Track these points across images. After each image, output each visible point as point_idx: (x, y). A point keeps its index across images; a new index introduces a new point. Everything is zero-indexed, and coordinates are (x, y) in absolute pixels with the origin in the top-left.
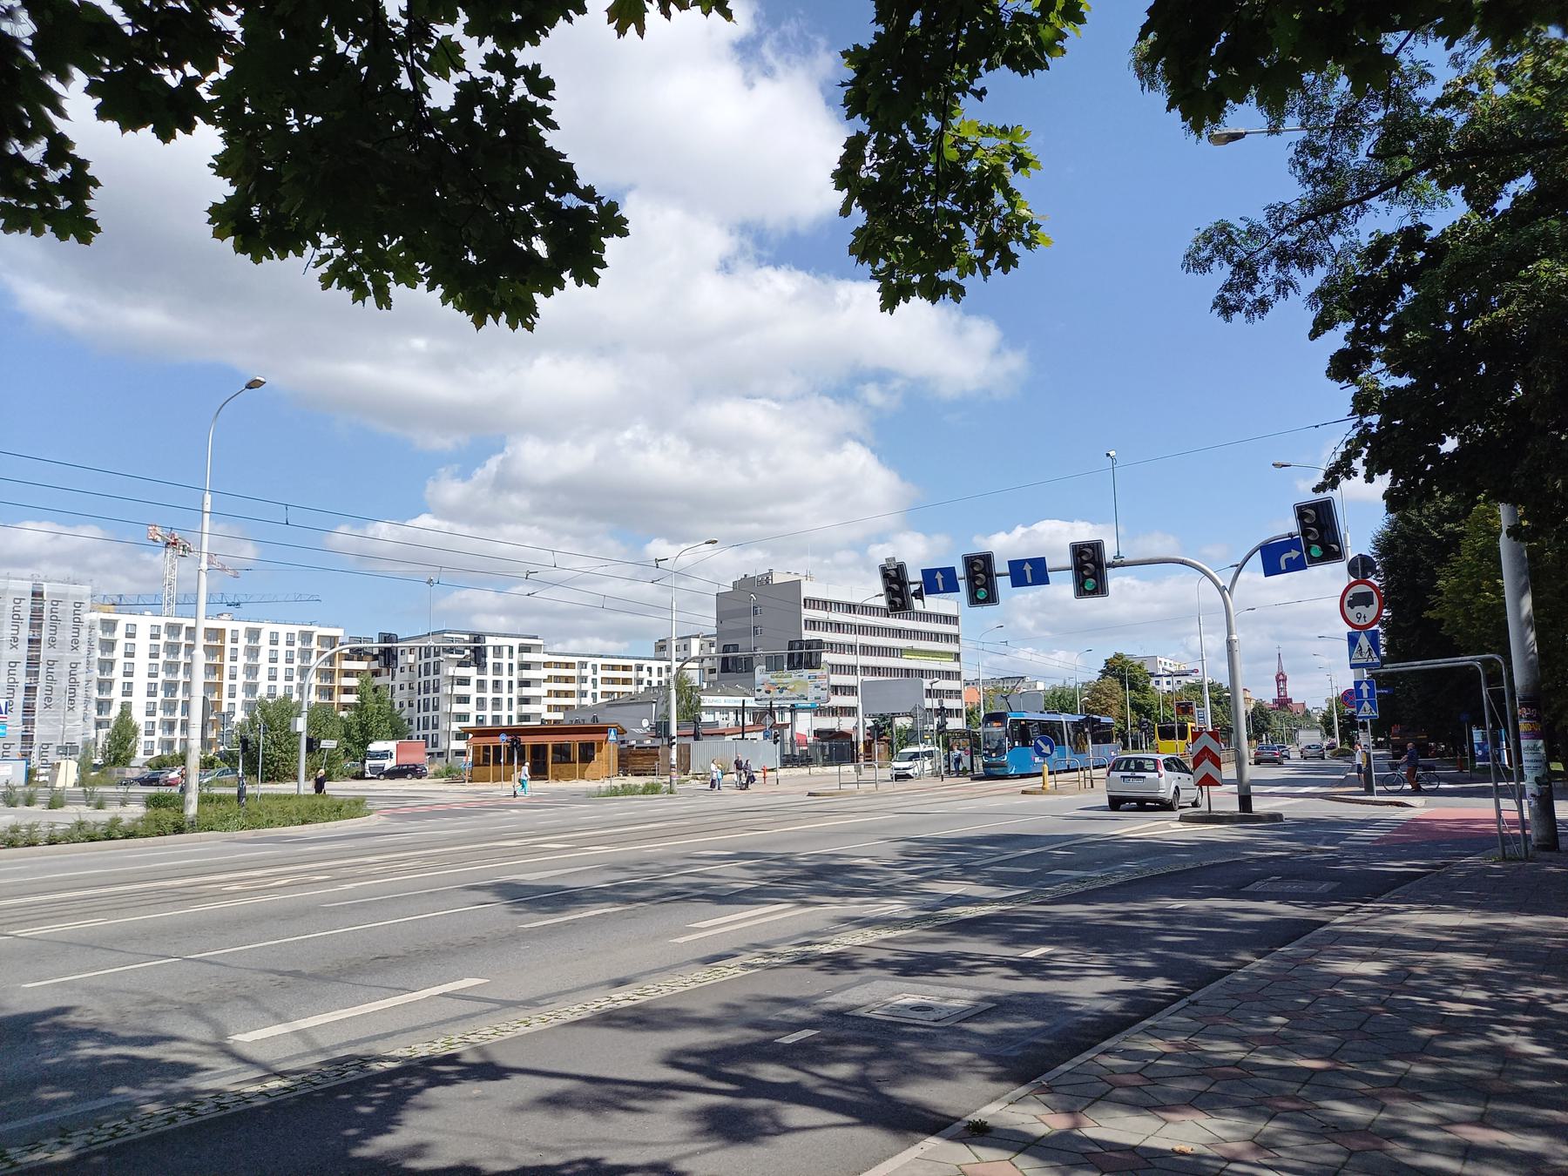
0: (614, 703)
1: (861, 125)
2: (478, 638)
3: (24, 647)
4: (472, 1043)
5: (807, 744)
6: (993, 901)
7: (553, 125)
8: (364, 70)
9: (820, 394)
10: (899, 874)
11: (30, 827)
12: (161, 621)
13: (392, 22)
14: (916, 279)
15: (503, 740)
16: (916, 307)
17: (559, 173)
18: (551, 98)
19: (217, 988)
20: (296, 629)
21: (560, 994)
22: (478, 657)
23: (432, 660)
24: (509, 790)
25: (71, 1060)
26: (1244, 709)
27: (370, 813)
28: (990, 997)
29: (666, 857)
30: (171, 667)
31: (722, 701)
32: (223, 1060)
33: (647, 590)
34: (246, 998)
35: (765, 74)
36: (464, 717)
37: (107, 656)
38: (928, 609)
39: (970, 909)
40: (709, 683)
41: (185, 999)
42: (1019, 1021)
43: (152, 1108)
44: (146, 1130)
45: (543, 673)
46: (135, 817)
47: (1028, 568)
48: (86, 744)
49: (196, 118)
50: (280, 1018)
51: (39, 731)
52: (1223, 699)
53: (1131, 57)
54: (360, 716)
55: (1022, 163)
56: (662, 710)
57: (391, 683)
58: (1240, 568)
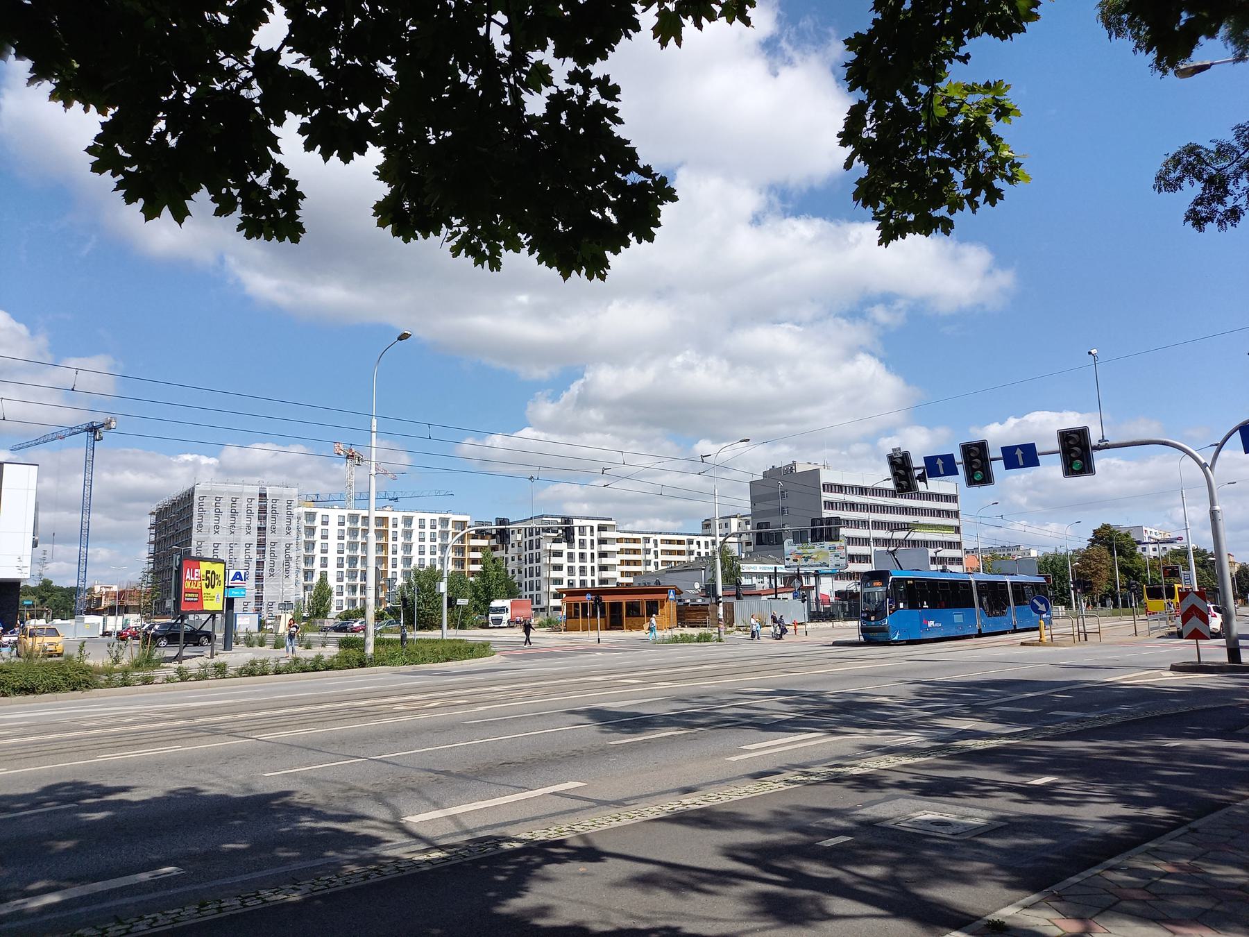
0: (672, 569)
1: (861, 95)
2: (567, 520)
3: (255, 532)
4: (577, 832)
5: (829, 603)
6: (1000, 736)
7: (619, 121)
8: (481, 92)
9: (836, 316)
10: (915, 711)
11: (263, 662)
12: (345, 513)
13: (499, 54)
14: (911, 218)
15: (588, 599)
16: (913, 242)
17: (625, 156)
18: (618, 100)
19: (393, 782)
20: (437, 517)
21: (641, 797)
22: (568, 535)
23: (534, 538)
24: (594, 637)
25: (296, 829)
26: (1229, 572)
27: (494, 653)
28: (1002, 816)
29: (718, 692)
30: (353, 546)
31: (758, 568)
32: (399, 835)
33: (695, 481)
34: (413, 789)
35: (786, 64)
36: (558, 581)
37: (310, 539)
38: (931, 490)
39: (979, 742)
40: (746, 554)
41: (371, 789)
42: (1029, 838)
43: (353, 868)
44: (349, 884)
45: (617, 547)
46: (332, 654)
47: (1019, 452)
48: (298, 601)
49: (368, 143)
50: (437, 805)
51: (267, 593)
52: (1208, 564)
53: (1098, 11)
54: (483, 581)
55: (1004, 112)
56: (710, 576)
57: (505, 556)
58: (1220, 446)
